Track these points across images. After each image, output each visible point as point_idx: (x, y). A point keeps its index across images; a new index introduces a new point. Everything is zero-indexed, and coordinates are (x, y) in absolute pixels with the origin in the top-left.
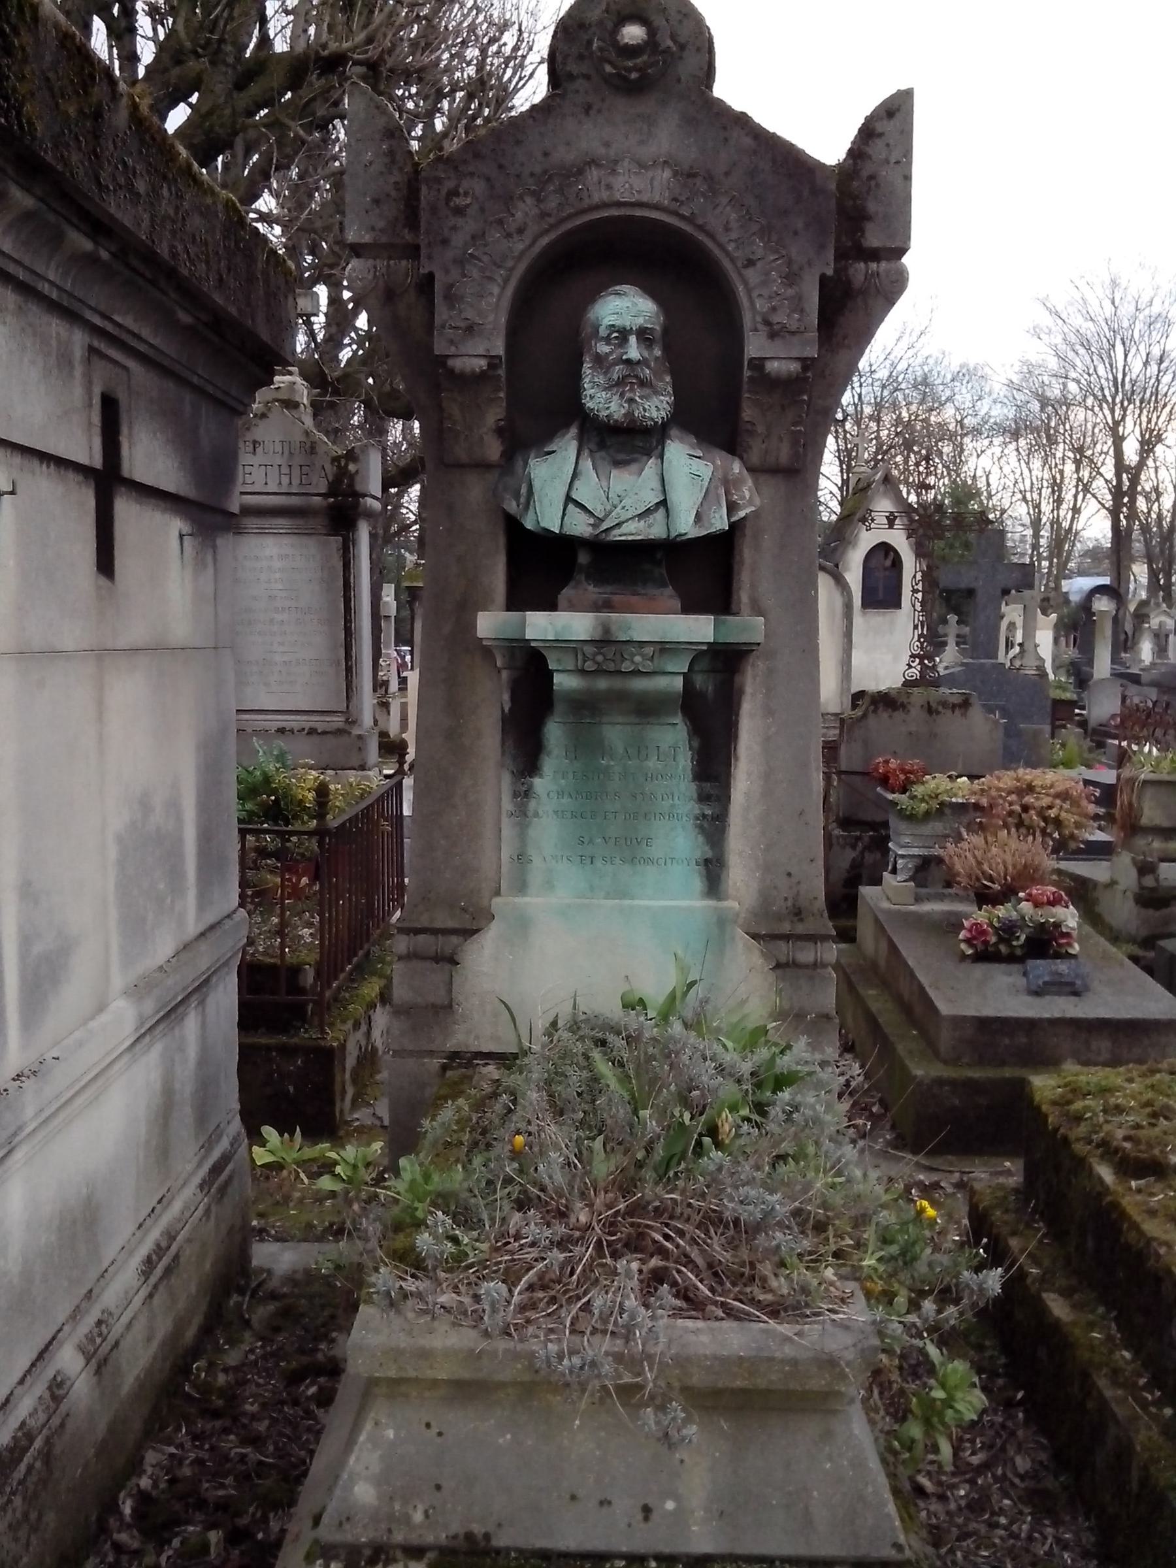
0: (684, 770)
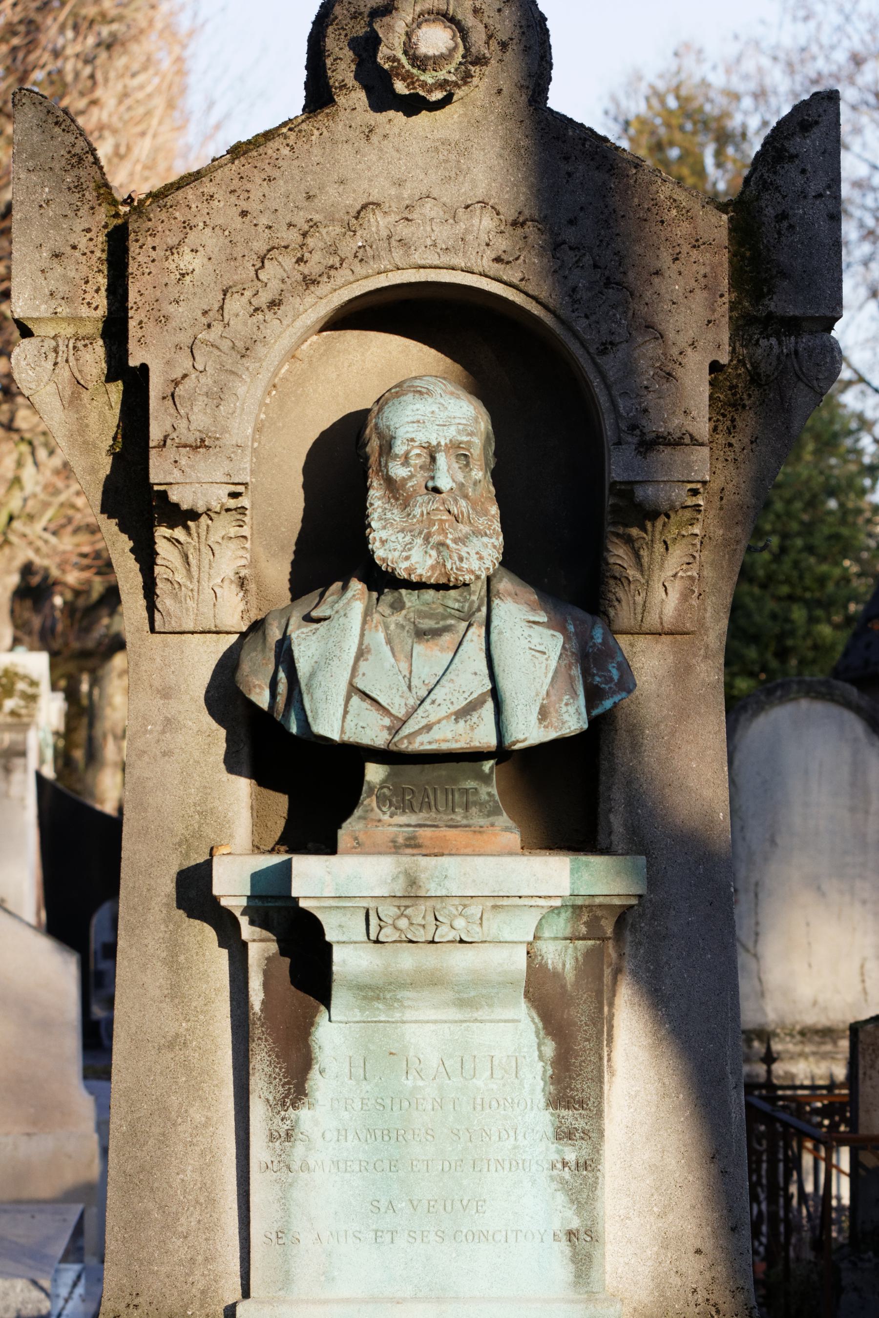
0: (532, 1091)
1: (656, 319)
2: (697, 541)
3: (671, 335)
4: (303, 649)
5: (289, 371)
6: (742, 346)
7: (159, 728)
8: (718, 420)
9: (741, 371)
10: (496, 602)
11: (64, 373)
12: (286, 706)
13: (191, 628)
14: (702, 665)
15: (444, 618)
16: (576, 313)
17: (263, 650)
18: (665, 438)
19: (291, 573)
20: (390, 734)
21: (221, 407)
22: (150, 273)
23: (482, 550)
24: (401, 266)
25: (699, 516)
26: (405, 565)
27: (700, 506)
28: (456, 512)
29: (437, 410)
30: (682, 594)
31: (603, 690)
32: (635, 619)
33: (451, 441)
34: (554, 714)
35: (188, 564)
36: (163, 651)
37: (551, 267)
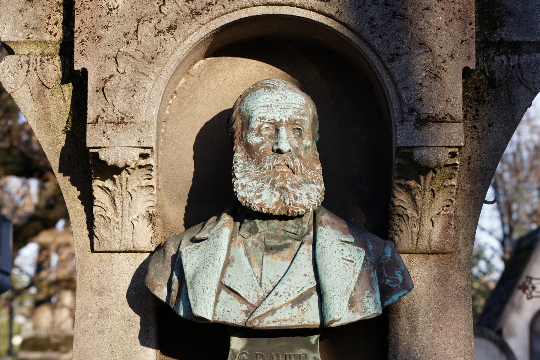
1: (427, 39)
2: (454, 190)
3: (437, 50)
4: (189, 259)
5: (185, 83)
6: (483, 61)
7: (96, 315)
8: (467, 111)
9: (483, 77)
10: (320, 228)
11: (34, 78)
12: (177, 298)
13: (117, 247)
14: (456, 274)
15: (285, 239)
16: (373, 35)
17: (164, 262)
18: (433, 118)
19: (185, 214)
20: (246, 316)
21: (135, 97)
22: (88, 9)
23: (310, 193)
24: (256, 3)
25: (456, 173)
26: (258, 201)
27: (457, 165)
28: (292, 166)
29: (280, 98)
30: (443, 227)
31: (392, 288)
32: (412, 243)
33: (289, 119)
34: (359, 303)
35: (115, 205)
36: (100, 264)
37: (356, 4)
